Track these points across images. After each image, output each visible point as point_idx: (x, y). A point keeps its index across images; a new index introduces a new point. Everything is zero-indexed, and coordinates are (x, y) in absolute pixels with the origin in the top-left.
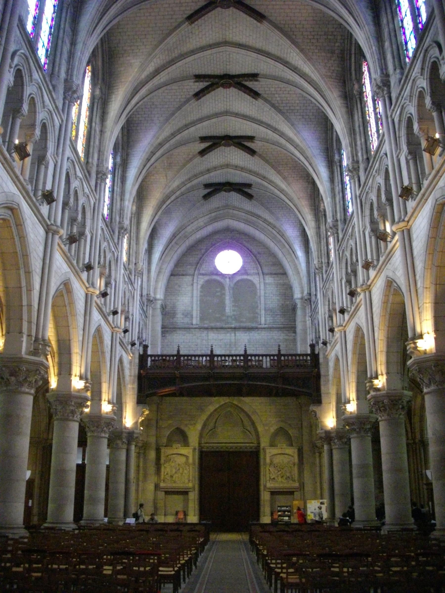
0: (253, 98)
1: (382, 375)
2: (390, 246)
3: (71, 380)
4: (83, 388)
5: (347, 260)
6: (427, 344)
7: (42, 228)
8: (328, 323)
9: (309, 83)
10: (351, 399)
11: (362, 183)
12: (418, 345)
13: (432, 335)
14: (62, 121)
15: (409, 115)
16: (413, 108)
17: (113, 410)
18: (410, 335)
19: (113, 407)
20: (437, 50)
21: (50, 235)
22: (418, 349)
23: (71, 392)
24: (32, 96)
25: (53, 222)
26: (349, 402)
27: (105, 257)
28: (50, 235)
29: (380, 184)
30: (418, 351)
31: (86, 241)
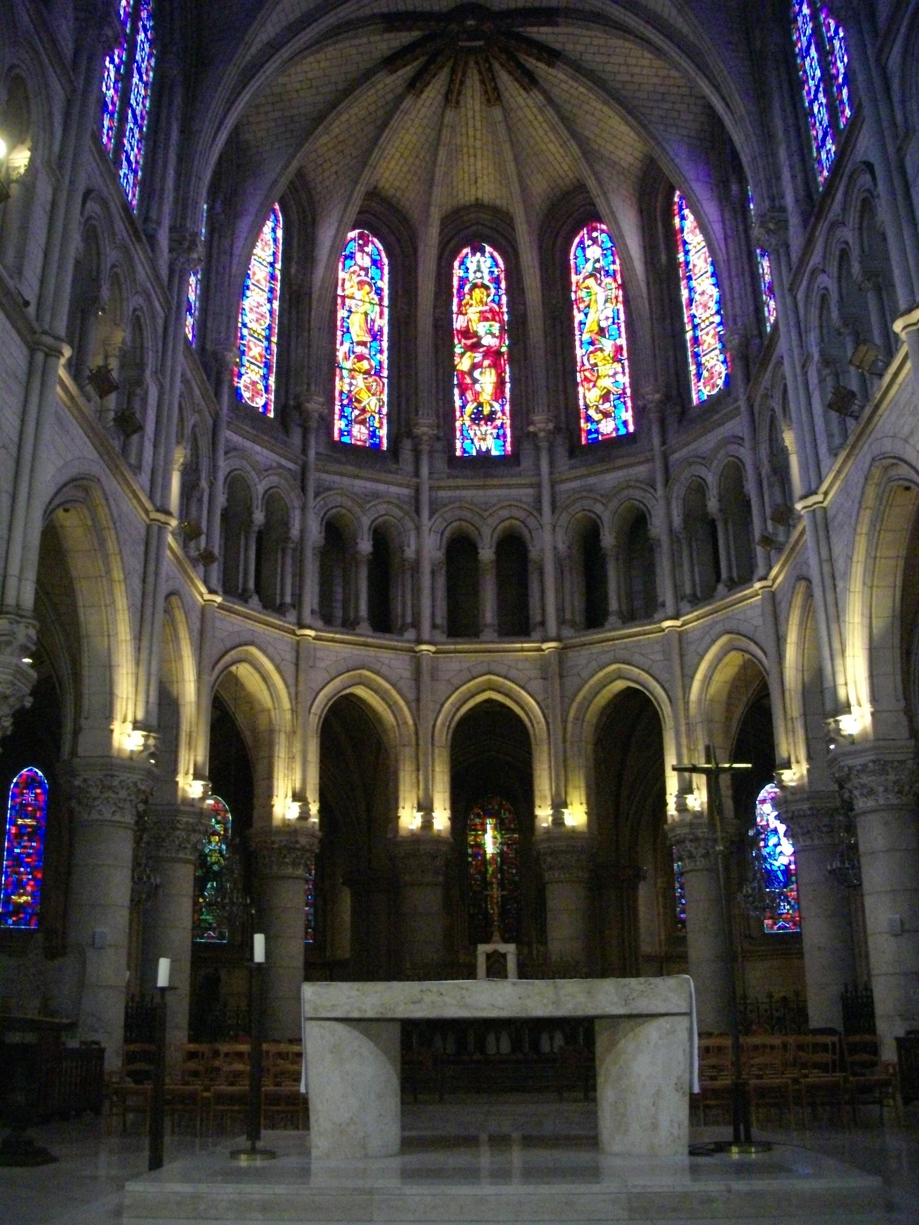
0: (506, 1184)
1: (798, 762)
2: (796, 534)
3: (112, 731)
4: (141, 748)
5: (785, 385)
6: (856, 722)
7: (17, 338)
8: (771, 495)
9: (666, 36)
10: (853, 701)
11: (794, 257)
12: (842, 726)
13: (867, 708)
14: (74, 90)
15: (844, 246)
16: (850, 234)
17: (145, 746)
18: (829, 706)
19: (146, 738)
20: (868, 177)
21: (40, 357)
22: (843, 733)
23: (175, 804)
24: (18, 71)
25: (47, 327)
26: (846, 708)
27: (181, 420)
28: (40, 357)
29: (847, 243)
30: (844, 736)
31: (200, 500)
